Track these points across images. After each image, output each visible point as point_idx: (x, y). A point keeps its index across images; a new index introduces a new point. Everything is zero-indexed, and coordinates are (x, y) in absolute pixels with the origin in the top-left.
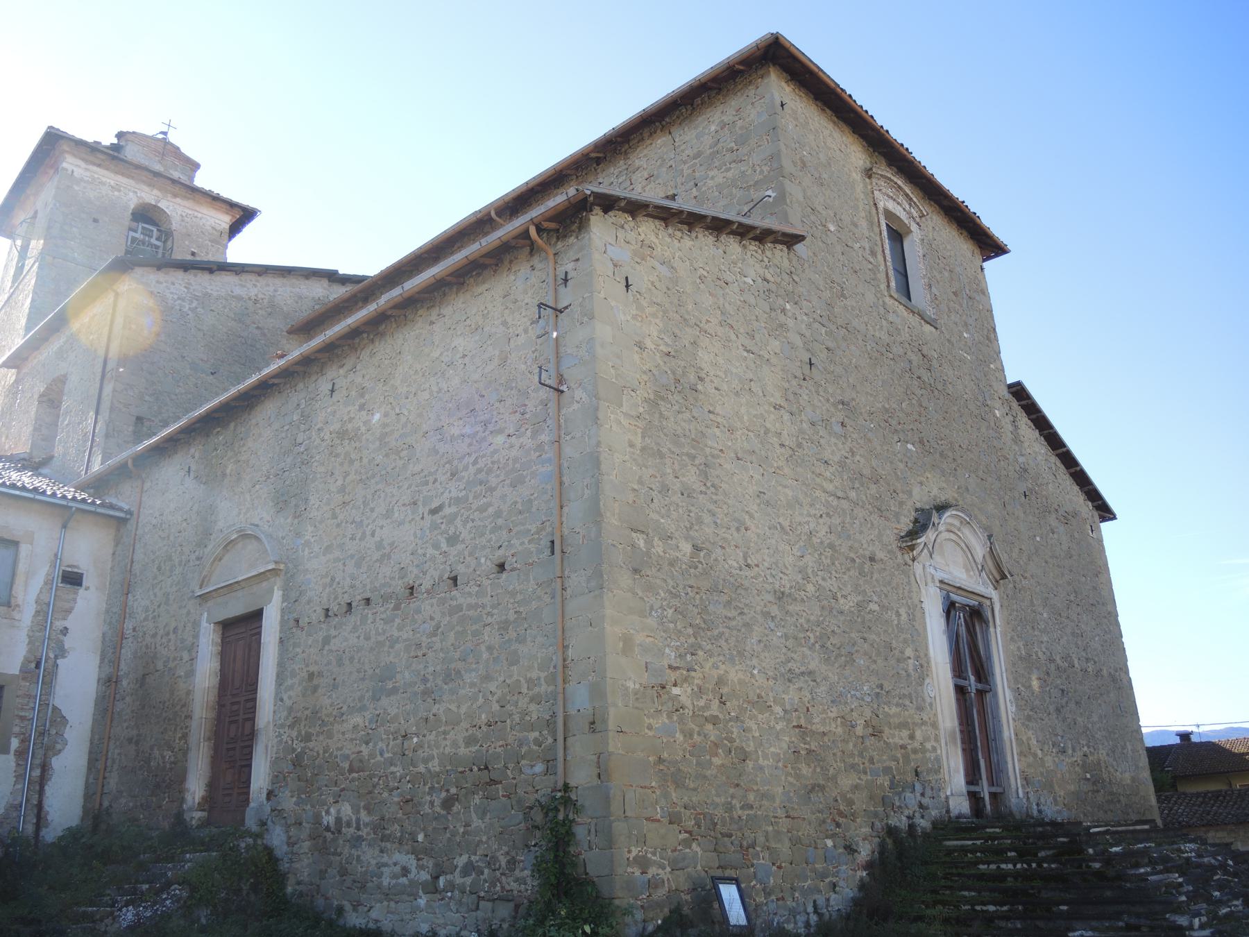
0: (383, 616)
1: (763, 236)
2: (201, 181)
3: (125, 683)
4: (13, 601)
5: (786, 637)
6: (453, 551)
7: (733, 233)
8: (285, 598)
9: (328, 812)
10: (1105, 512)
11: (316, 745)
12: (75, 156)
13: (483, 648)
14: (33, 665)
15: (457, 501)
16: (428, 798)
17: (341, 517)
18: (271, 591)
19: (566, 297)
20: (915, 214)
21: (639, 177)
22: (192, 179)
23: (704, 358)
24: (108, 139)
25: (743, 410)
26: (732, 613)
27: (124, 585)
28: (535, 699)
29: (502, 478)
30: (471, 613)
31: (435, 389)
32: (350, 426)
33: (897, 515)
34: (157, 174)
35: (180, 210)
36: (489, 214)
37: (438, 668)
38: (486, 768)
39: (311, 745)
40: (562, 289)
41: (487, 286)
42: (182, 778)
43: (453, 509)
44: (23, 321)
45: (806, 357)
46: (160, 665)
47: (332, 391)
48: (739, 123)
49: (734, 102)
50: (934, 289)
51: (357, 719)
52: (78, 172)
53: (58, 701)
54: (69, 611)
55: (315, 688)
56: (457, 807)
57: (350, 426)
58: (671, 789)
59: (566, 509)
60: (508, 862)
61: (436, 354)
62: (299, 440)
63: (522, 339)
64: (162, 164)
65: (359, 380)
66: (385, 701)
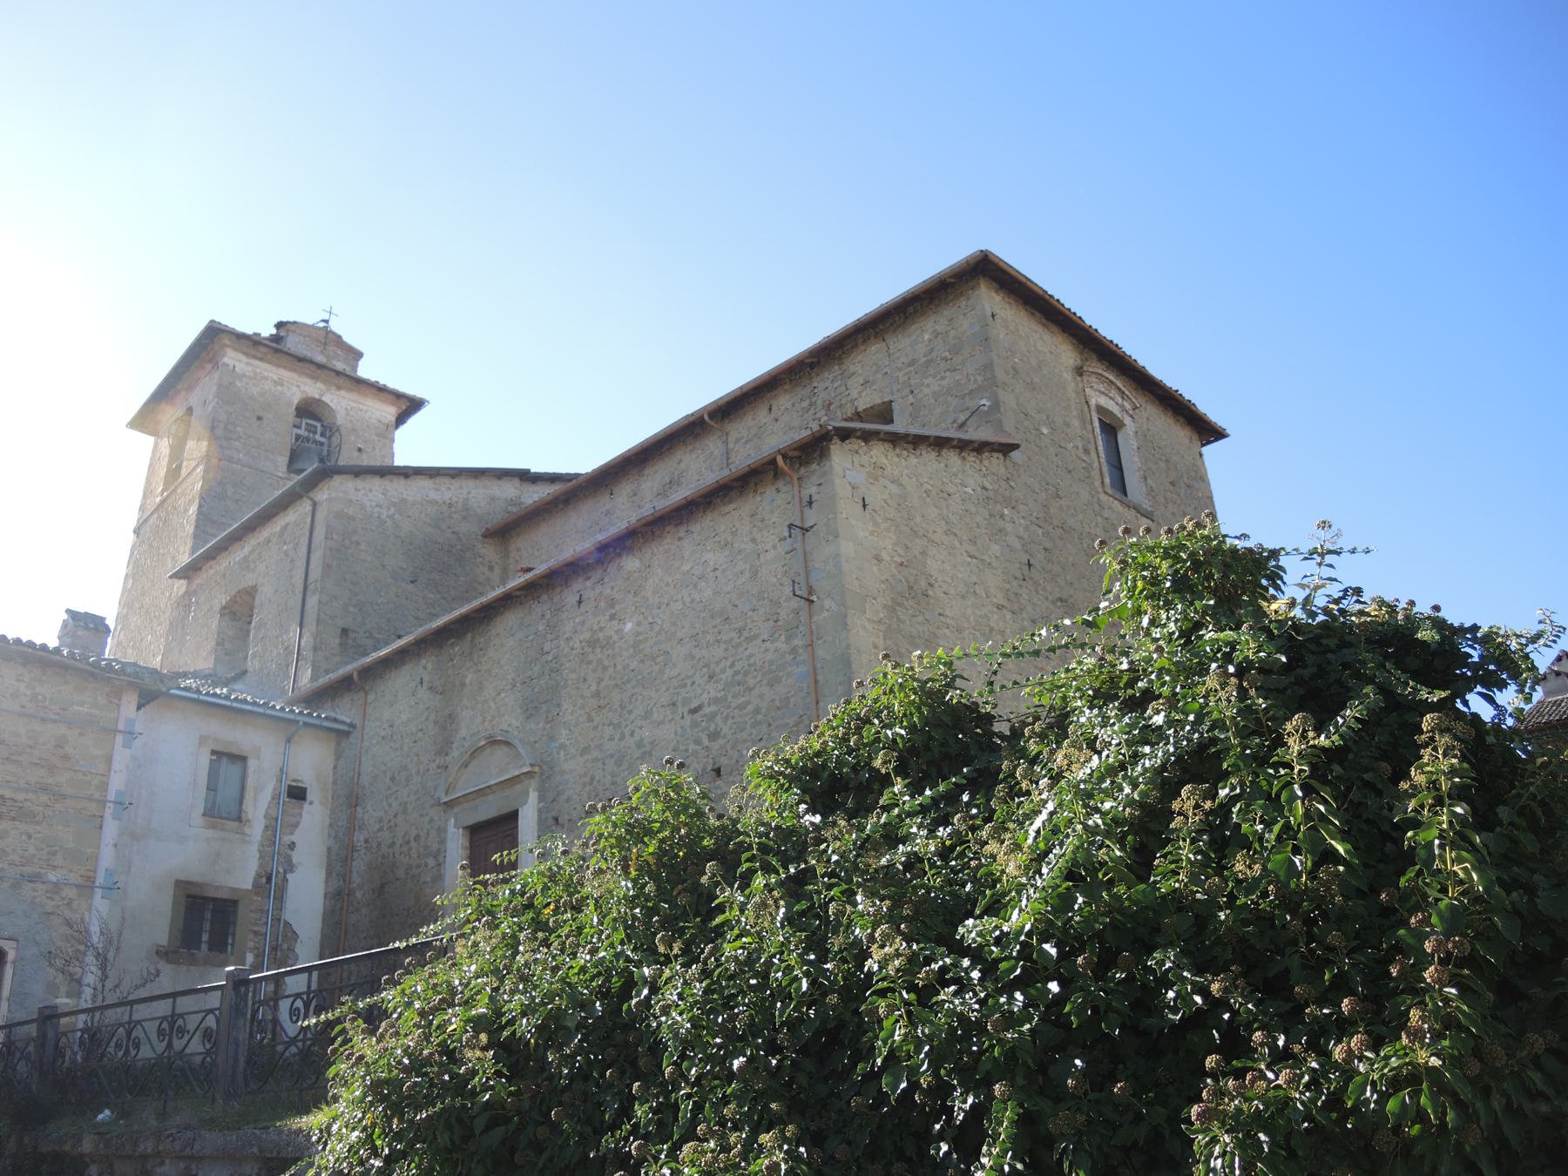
1: (981, 448)
2: (365, 370)
3: (358, 894)
6: (715, 746)
7: (954, 447)
8: (541, 798)
15: (716, 701)
17: (597, 720)
18: (526, 793)
19: (811, 517)
20: (1127, 406)
21: (854, 384)
22: (355, 369)
23: (933, 566)
25: (969, 611)
27: (349, 799)
31: (687, 600)
34: (320, 366)
36: (702, 418)
40: (807, 511)
41: (733, 506)
43: (713, 708)
44: (190, 529)
46: (401, 873)
47: (580, 602)
48: (952, 333)
49: (947, 312)
50: (1149, 481)
53: (288, 915)
54: (295, 826)
61: (686, 568)
62: (547, 647)
63: (771, 555)
65: (608, 591)
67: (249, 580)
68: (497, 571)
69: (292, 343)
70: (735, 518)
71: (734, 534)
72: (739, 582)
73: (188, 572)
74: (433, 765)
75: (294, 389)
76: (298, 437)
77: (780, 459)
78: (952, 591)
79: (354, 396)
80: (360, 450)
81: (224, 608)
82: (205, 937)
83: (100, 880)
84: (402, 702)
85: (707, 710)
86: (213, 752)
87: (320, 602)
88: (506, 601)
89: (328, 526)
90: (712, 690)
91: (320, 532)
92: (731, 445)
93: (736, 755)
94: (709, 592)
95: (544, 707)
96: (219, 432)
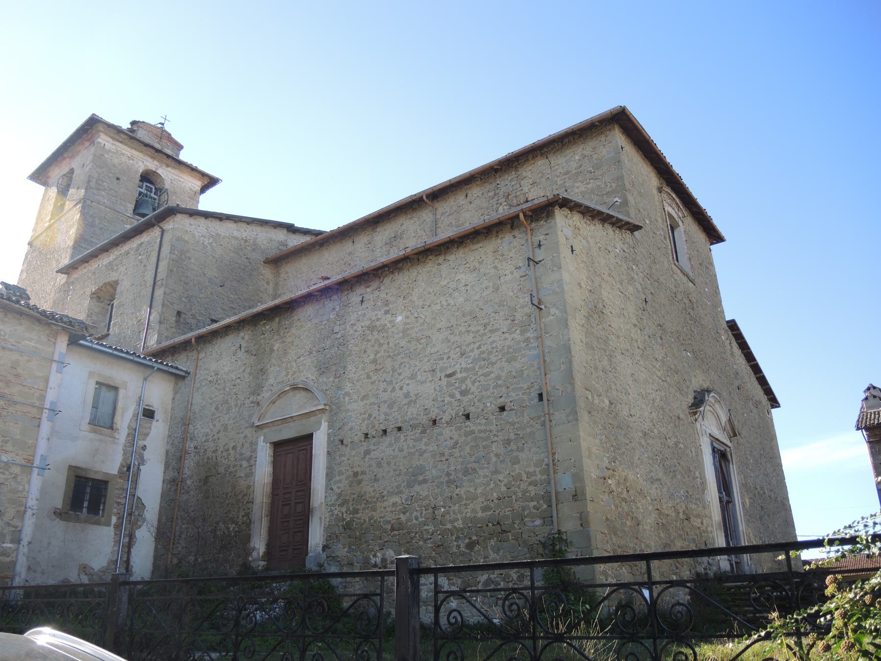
0: (414, 437)
2: (183, 156)
3: (189, 482)
4: (114, 426)
5: (648, 457)
6: (466, 399)
8: (330, 427)
9: (375, 556)
10: (774, 402)
11: (364, 516)
12: (106, 134)
13: (492, 455)
14: (125, 469)
16: (456, 543)
18: (319, 423)
22: (178, 155)
23: (605, 294)
24: (125, 125)
26: (627, 442)
28: (534, 484)
29: (500, 356)
30: (482, 435)
31: (444, 303)
32: (378, 323)
33: (687, 393)
37: (459, 467)
38: (498, 523)
39: (358, 516)
40: (537, 251)
41: (480, 245)
42: (248, 538)
43: (464, 375)
45: (643, 297)
46: (221, 470)
47: (362, 301)
48: (595, 156)
51: (396, 499)
52: (108, 146)
53: (140, 493)
54: (147, 435)
55: (360, 482)
56: (477, 548)
57: (378, 323)
58: (613, 536)
59: (548, 376)
60: (519, 577)
61: (444, 283)
64: (158, 144)
65: (383, 296)
66: (417, 488)
67: (113, 277)
68: (271, 285)
69: (141, 134)
70: (482, 254)
71: (481, 263)
72: (484, 294)
73: (67, 270)
74: (248, 401)
76: (140, 193)
77: (521, 216)
78: (614, 312)
81: (94, 294)
82: (86, 504)
83: (37, 462)
84: (224, 361)
85: (459, 375)
86: (97, 383)
87: (165, 293)
88: (308, 298)
89: (172, 245)
90: (464, 363)
91: (166, 249)
92: (438, 216)
93: (481, 406)
94: (461, 299)
95: (334, 368)
96: (93, 184)
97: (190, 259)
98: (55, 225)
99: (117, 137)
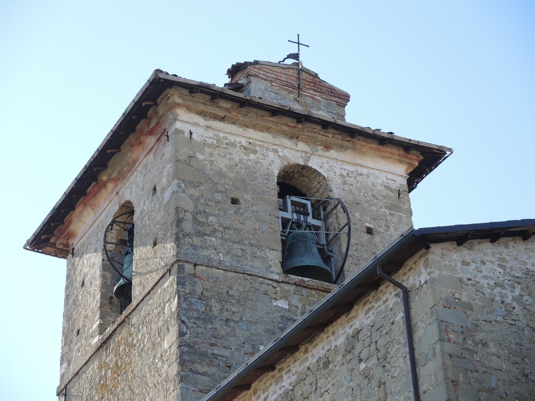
2: (354, 116)
12: (189, 109)
22: (342, 117)
24: (220, 80)
35: (338, 168)
52: (199, 134)
69: (258, 90)
75: (271, 154)
76: (285, 222)
79: (347, 156)
80: (369, 231)
89: (440, 322)
91: (427, 334)
97: (485, 345)
98: (118, 338)
99: (212, 110)
